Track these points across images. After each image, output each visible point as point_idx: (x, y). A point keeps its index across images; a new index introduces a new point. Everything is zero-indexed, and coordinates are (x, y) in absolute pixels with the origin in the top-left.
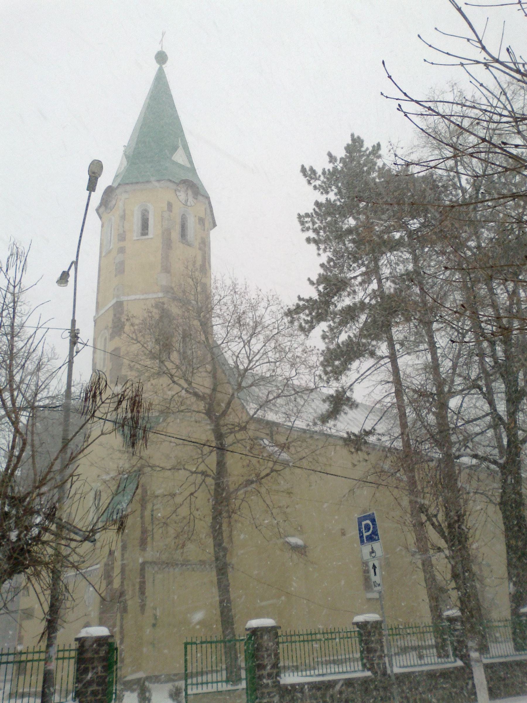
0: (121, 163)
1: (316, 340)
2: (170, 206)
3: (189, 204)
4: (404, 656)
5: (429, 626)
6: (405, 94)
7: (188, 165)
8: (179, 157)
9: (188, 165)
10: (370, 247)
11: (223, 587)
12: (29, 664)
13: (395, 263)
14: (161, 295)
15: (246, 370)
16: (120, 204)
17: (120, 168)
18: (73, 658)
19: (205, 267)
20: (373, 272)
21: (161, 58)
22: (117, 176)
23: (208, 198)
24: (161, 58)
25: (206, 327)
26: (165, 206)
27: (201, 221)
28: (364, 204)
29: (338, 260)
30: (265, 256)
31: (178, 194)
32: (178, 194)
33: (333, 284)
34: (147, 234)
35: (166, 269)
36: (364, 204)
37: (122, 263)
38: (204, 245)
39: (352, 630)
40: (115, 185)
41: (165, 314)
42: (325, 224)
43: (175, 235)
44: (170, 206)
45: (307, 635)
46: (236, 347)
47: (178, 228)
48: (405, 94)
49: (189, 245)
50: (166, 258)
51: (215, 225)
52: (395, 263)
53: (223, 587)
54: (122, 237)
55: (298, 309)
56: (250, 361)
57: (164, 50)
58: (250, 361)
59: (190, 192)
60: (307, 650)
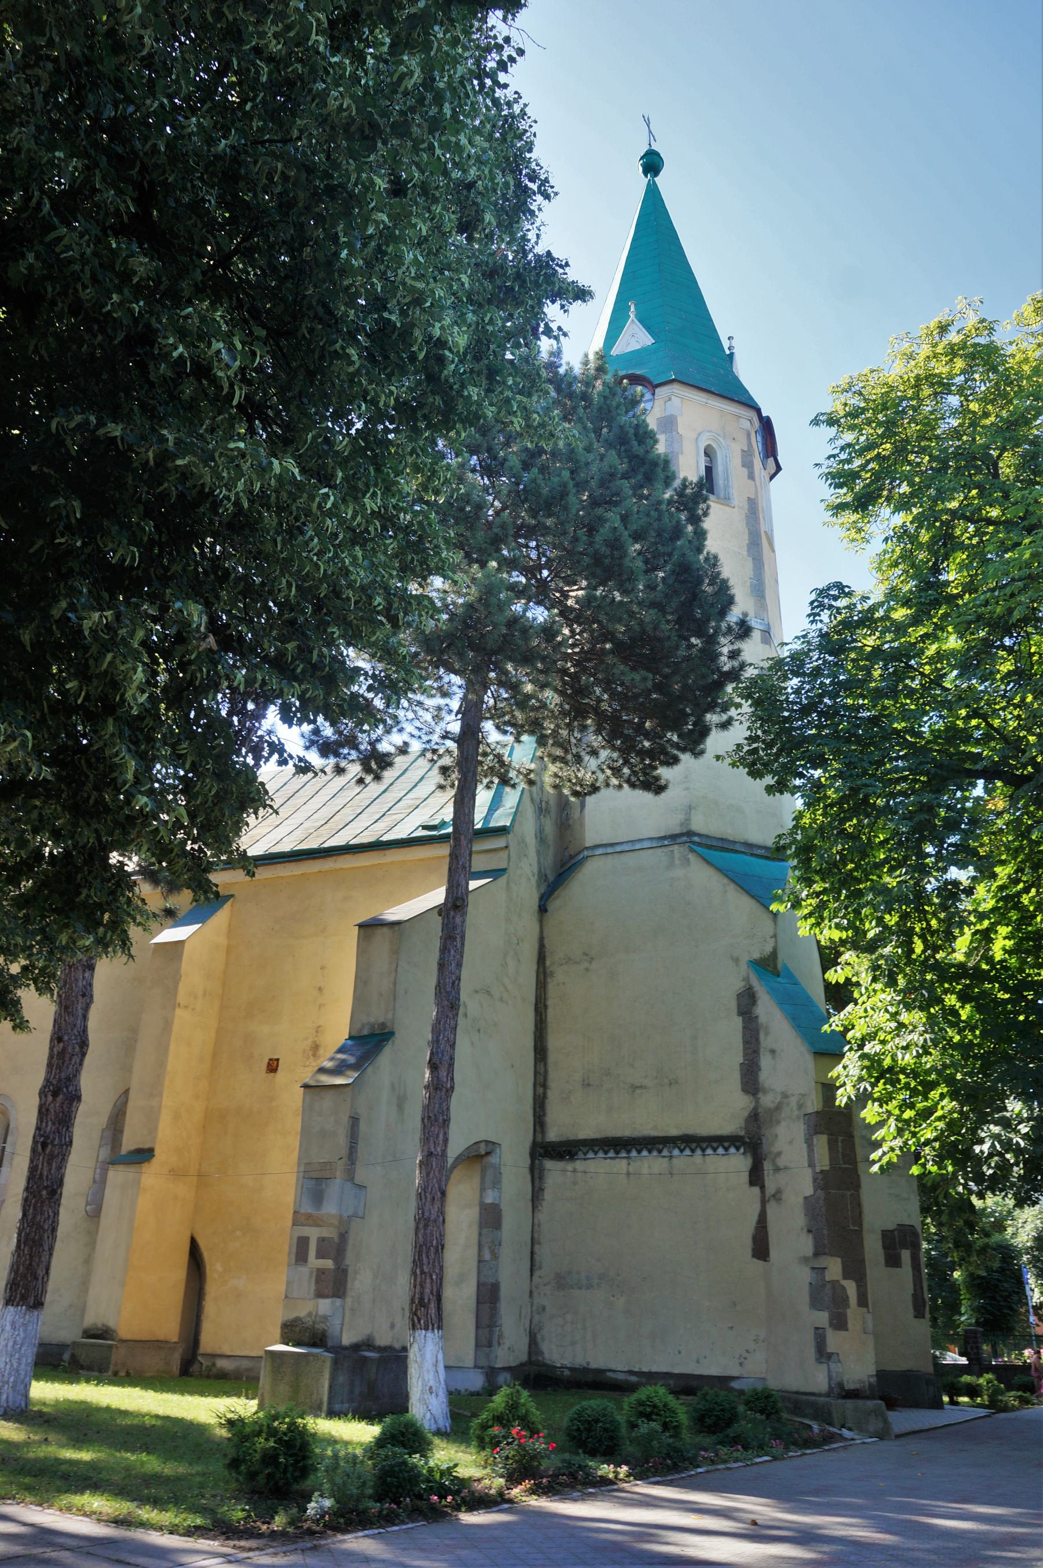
24: (652, 164)
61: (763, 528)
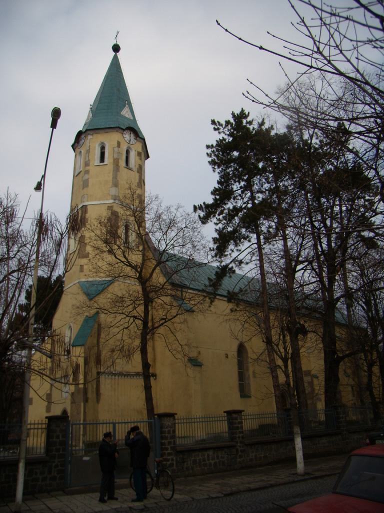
0: (89, 116)
1: (210, 231)
2: (119, 144)
3: (131, 143)
4: (217, 432)
5: (224, 417)
6: (316, 11)
7: (132, 118)
8: (125, 112)
9: (132, 118)
10: (247, 170)
11: (148, 388)
12: (32, 431)
13: (262, 185)
14: (111, 201)
15: (164, 251)
16: (87, 142)
17: (88, 119)
18: (28, 424)
19: (141, 183)
20: (248, 187)
21: (116, 48)
22: (85, 124)
23: (144, 140)
24: (116, 48)
25: (140, 222)
26: (116, 145)
27: (139, 154)
28: (242, 148)
29: (225, 180)
30: (179, 180)
31: (124, 136)
32: (124, 136)
33: (223, 193)
34: (104, 162)
35: (116, 185)
36: (242, 148)
37: (87, 181)
38: (141, 170)
39: (223, 415)
40: (84, 130)
41: (115, 214)
42: (221, 155)
43: (122, 163)
44: (119, 144)
45: (255, 415)
46: (159, 235)
47: (124, 158)
48: (316, 11)
49: (131, 169)
50: (115, 177)
51: (148, 157)
52: (262, 185)
53: (148, 388)
54: (87, 164)
55: (201, 208)
56: (167, 246)
57: (118, 43)
58: (167, 246)
59: (132, 135)
60: (193, 427)
61: (143, 178)
